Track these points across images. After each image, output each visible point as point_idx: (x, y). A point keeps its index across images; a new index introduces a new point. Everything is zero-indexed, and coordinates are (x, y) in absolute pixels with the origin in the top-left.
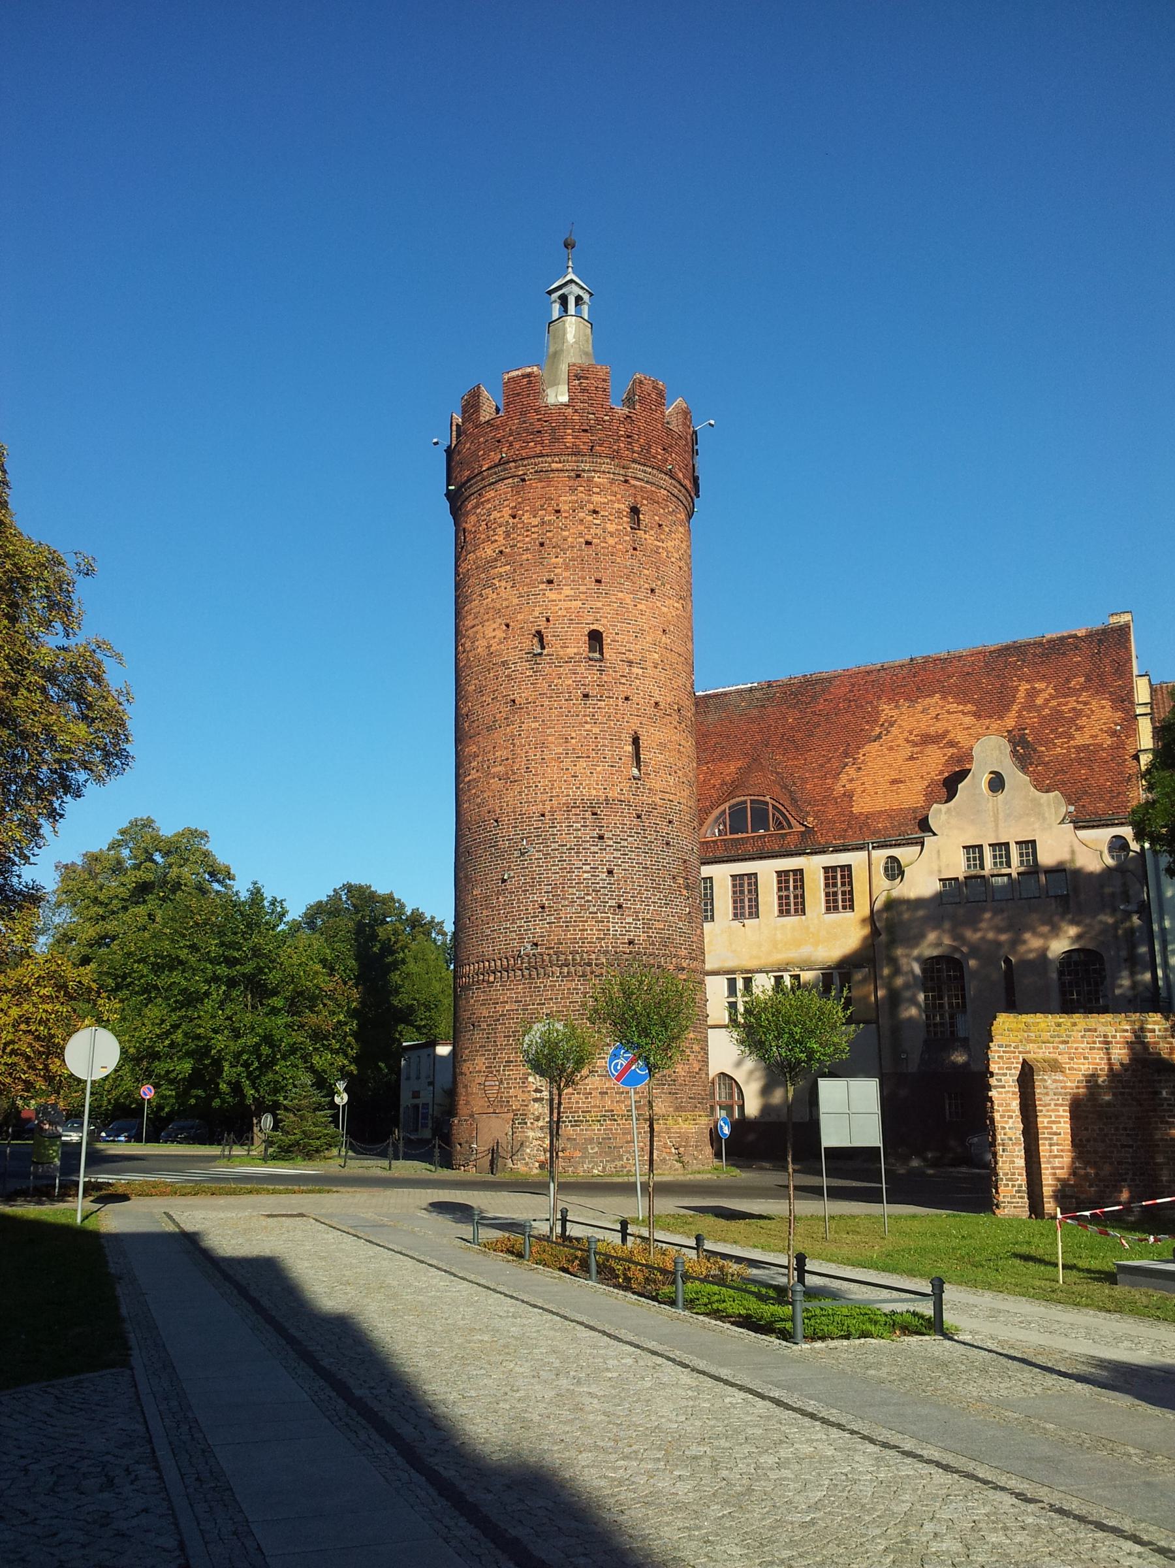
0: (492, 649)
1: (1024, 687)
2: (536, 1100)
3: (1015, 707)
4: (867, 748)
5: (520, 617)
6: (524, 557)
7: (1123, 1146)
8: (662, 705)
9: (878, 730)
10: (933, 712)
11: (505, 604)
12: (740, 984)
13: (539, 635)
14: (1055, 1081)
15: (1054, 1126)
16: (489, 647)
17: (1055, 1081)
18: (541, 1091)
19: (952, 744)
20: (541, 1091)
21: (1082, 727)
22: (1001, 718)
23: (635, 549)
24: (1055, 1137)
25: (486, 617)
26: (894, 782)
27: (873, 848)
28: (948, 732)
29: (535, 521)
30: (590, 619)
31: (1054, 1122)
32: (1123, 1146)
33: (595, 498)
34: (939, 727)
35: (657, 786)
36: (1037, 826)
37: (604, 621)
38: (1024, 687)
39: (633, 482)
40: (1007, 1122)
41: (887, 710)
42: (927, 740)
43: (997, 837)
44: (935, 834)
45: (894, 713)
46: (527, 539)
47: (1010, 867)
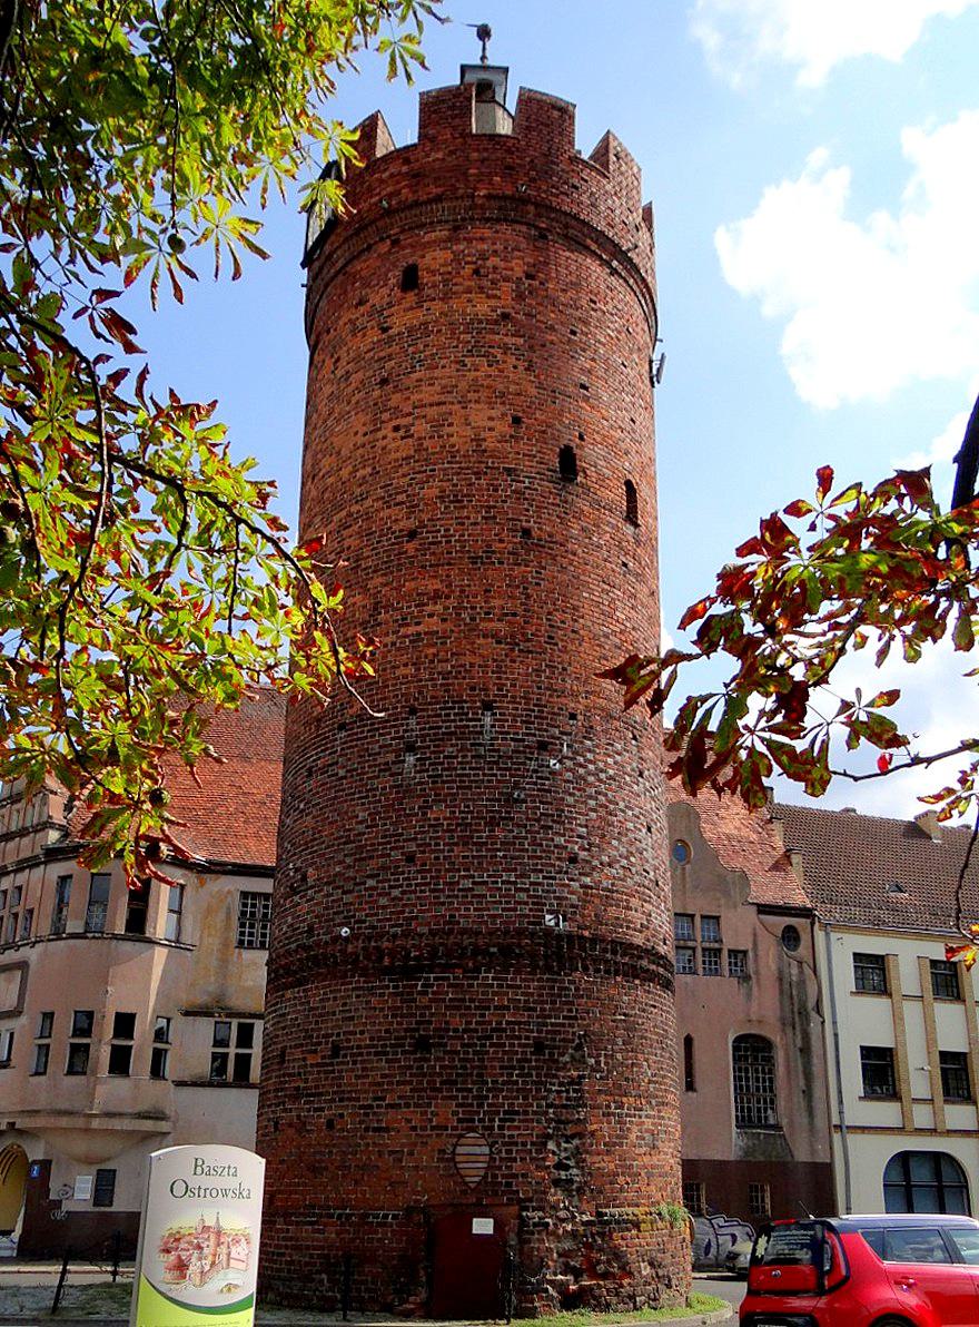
2: (557, 1183)
20: (567, 1168)
36: (723, 901)
43: (684, 908)
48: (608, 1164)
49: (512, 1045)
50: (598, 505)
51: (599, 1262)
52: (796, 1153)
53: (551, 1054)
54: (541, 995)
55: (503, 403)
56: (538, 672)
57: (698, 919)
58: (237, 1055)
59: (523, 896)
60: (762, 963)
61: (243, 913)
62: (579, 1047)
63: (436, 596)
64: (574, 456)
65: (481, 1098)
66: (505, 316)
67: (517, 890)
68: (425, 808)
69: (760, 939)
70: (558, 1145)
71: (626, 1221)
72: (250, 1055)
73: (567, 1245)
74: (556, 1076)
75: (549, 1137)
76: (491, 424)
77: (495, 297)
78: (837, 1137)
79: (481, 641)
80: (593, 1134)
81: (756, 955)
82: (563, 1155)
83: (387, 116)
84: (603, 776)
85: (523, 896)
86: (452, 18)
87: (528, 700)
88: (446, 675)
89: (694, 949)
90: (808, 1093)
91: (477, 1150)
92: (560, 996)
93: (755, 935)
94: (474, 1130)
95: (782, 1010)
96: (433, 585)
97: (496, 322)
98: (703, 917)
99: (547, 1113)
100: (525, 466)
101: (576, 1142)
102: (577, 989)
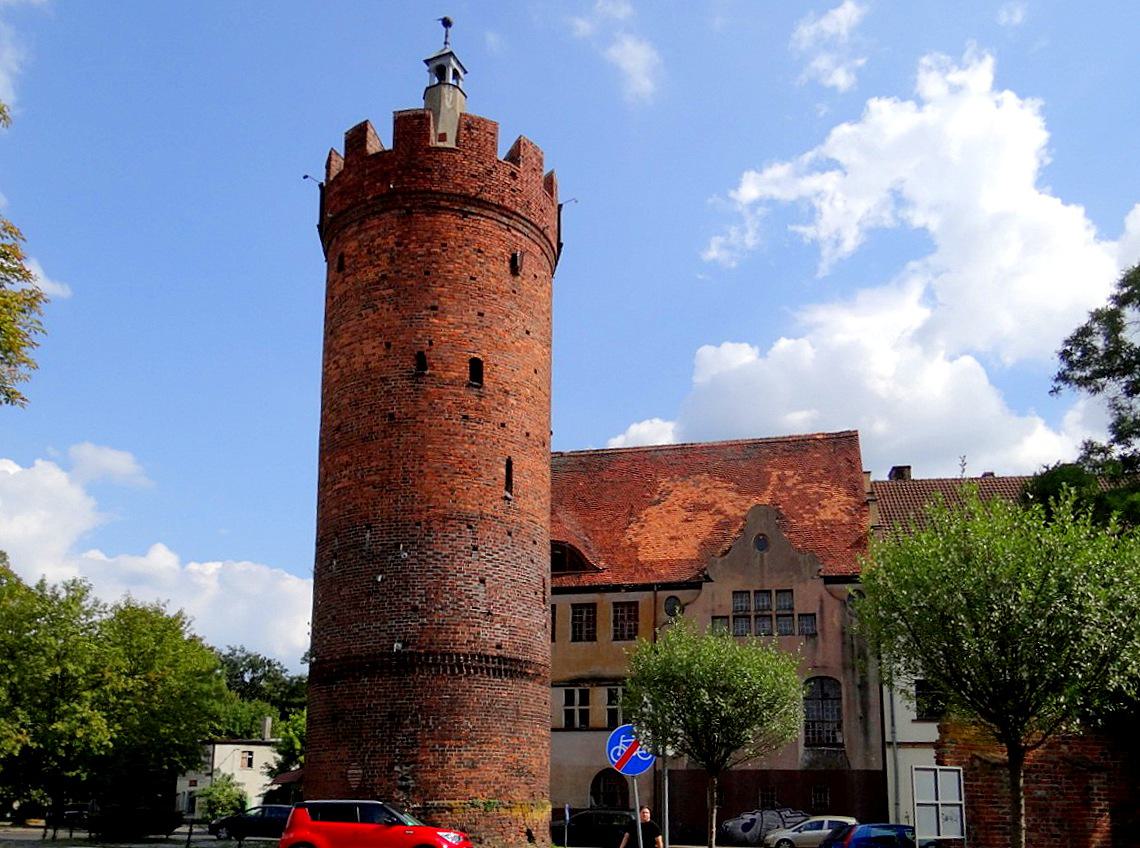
0: (372, 365)
1: (775, 473)
2: (401, 788)
4: (649, 510)
5: (402, 337)
6: (409, 283)
7: (1053, 836)
8: (532, 436)
9: (657, 497)
10: (703, 486)
16: (367, 363)
18: (408, 779)
19: (719, 512)
21: (824, 507)
22: (759, 495)
25: (365, 335)
27: (659, 589)
28: (716, 502)
32: (1053, 836)
34: (709, 499)
35: (526, 508)
36: (795, 577)
37: (485, 352)
38: (775, 473)
41: (664, 483)
42: (698, 507)
43: (763, 586)
44: (712, 581)
46: (412, 267)
47: (748, 592)
48: (432, 778)
49: (376, 716)
50: (443, 384)
52: (852, 764)
53: (399, 720)
54: (393, 688)
55: (380, 336)
56: (396, 502)
57: (752, 594)
58: (574, 710)
59: (384, 634)
60: (828, 621)
61: (616, 617)
62: (416, 715)
63: (348, 465)
64: (424, 357)
65: (360, 745)
66: (384, 277)
67: (381, 631)
68: (340, 589)
69: (825, 603)
70: (401, 768)
72: (588, 710)
75: (396, 764)
76: (374, 351)
77: (379, 265)
78: (889, 752)
79: (366, 489)
80: (423, 762)
81: (822, 618)
82: (405, 773)
83: (373, 122)
84: (439, 557)
85: (384, 634)
87: (389, 519)
88: (349, 511)
89: (771, 616)
90: (864, 719)
91: (356, 772)
92: (404, 687)
93: (822, 601)
94: (355, 761)
95: (843, 656)
96: (345, 458)
97: (378, 283)
98: (777, 592)
99: (394, 752)
100: (393, 374)
101: (412, 766)
102: (415, 683)
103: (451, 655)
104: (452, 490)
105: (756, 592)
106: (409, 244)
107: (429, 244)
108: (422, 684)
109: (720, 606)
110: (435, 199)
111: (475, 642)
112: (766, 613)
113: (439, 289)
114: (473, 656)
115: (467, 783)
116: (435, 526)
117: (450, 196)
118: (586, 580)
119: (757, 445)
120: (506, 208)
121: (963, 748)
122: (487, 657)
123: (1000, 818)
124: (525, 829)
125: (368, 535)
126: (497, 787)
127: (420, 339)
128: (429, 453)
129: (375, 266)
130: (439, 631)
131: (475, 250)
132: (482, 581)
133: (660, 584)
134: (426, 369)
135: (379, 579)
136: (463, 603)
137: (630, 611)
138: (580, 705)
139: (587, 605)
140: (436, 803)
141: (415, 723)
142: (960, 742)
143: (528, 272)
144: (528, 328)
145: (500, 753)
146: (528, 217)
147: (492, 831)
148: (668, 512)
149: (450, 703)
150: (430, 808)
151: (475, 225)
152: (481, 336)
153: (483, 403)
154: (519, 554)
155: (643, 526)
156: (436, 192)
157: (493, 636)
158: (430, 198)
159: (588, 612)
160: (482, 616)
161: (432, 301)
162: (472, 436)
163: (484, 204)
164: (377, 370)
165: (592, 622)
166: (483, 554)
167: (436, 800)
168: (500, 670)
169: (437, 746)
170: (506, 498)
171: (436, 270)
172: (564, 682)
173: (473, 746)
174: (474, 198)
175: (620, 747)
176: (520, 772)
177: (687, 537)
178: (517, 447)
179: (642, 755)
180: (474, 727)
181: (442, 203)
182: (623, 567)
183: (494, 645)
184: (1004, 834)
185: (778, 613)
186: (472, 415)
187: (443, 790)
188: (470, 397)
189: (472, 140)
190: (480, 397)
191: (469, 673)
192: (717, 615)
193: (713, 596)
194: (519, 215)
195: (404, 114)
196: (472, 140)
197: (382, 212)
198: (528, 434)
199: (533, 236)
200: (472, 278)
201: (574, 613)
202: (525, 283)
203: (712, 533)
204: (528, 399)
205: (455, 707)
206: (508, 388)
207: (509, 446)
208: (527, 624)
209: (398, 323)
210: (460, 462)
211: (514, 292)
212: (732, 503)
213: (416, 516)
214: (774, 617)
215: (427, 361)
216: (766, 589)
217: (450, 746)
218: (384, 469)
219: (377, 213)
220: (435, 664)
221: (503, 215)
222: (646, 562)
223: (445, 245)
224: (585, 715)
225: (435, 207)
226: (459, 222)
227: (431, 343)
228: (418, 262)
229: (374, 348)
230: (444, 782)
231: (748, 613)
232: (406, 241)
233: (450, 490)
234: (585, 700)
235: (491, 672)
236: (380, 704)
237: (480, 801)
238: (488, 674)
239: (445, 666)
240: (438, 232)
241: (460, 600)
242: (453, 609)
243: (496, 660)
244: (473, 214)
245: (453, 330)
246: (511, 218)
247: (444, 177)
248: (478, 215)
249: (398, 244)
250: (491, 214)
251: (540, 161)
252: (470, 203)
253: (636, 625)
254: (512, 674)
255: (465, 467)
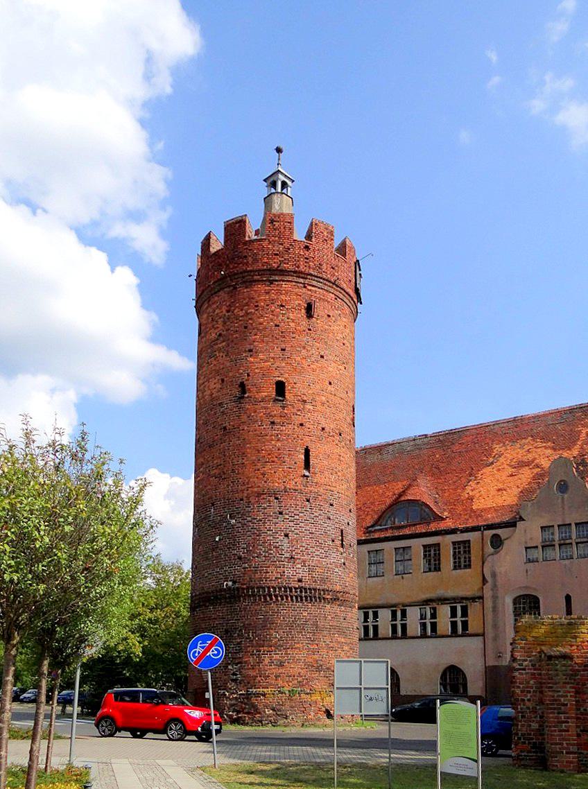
3: (579, 443)
4: (484, 470)
5: (231, 374)
8: (327, 429)
9: (491, 460)
10: (526, 448)
11: (222, 367)
12: (399, 614)
13: (242, 385)
14: (564, 665)
15: (562, 699)
17: (564, 665)
18: (236, 675)
19: (537, 466)
20: (236, 675)
22: (570, 449)
23: (310, 330)
24: (563, 708)
25: (210, 376)
26: (499, 490)
27: (484, 529)
28: (535, 459)
29: (241, 313)
30: (277, 373)
31: (562, 696)
33: (283, 297)
34: (530, 457)
35: (322, 481)
39: (309, 288)
40: (526, 696)
41: (497, 448)
42: (522, 464)
45: (502, 449)
47: (553, 526)
48: (251, 673)
50: (257, 402)
51: (245, 708)
53: (231, 634)
56: (228, 486)
59: (221, 576)
61: (455, 553)
62: (241, 630)
71: (258, 694)
73: (233, 702)
74: (232, 642)
75: (229, 664)
80: (246, 662)
84: (255, 521)
85: (221, 576)
86: (114, 274)
87: (224, 498)
89: (571, 544)
97: (217, 339)
98: (577, 524)
103: (264, 588)
104: (264, 474)
105: (559, 526)
106: (234, 310)
107: (246, 307)
108: (245, 609)
109: (531, 539)
110: (250, 275)
111: (280, 578)
112: (568, 541)
113: (253, 337)
114: (280, 588)
115: (276, 677)
116: (252, 500)
117: (261, 272)
118: (433, 527)
119: (571, 410)
120: (302, 273)
121: (534, 644)
122: (291, 589)
123: (556, 700)
124: (324, 709)
125: (212, 510)
126: (300, 679)
127: (242, 374)
128: (248, 450)
129: (215, 329)
130: (256, 572)
131: (278, 305)
132: (286, 535)
133: (485, 526)
134: (245, 393)
135: (217, 539)
136: (272, 552)
137: (465, 547)
138: (462, 617)
139: (464, 542)
140: (255, 690)
141: (240, 636)
142: (530, 639)
143: (321, 313)
144: (322, 353)
145: (302, 655)
146: (320, 275)
147: (295, 711)
148: (499, 470)
149: (263, 621)
150: (250, 694)
151: (279, 288)
152: (284, 364)
153: (286, 411)
154: (316, 514)
155: (479, 483)
156: (251, 271)
157: (294, 573)
158: (247, 276)
159: (435, 550)
160: (286, 560)
161: (248, 346)
162: (277, 435)
163: (283, 272)
164: (218, 398)
165: (438, 557)
166: (287, 517)
167: (255, 688)
168: (301, 597)
169: (255, 651)
170: (304, 476)
171: (252, 324)
172: (418, 602)
173: (280, 651)
174: (277, 270)
175: (198, 650)
176: (319, 669)
177: (510, 488)
178: (313, 438)
179: (214, 655)
180: (281, 637)
181: (255, 277)
182: (461, 515)
183: (296, 579)
184: (559, 713)
185: (577, 541)
186: (277, 420)
187: (259, 682)
188: (276, 409)
189: (275, 229)
190: (283, 408)
191: (277, 600)
192: (529, 545)
193: (525, 531)
194: (311, 275)
195: (230, 222)
196: (275, 229)
197: (219, 291)
198: (323, 429)
199: (326, 288)
200: (276, 326)
201: (425, 551)
202: (319, 322)
203: (530, 483)
204: (323, 404)
205: (267, 624)
206: (305, 398)
207: (307, 439)
208: (325, 563)
209: (228, 364)
210: (269, 454)
211: (310, 330)
212: (545, 457)
213: (240, 495)
214: (574, 544)
215: (247, 387)
216: (567, 523)
217: (264, 652)
218: (221, 465)
219: (215, 293)
220: (254, 595)
221: (299, 277)
222: (478, 509)
223: (257, 306)
224: (434, 626)
225: (250, 282)
226: (267, 288)
227: (248, 375)
228: (240, 320)
229: (215, 384)
230: (260, 676)
231: (554, 543)
232: (233, 308)
233: (262, 474)
234: (465, 613)
235: (294, 598)
236: (220, 624)
237: (286, 689)
238: (292, 600)
239: (260, 596)
240: (253, 298)
241: (271, 550)
242: (265, 556)
243: (298, 590)
244: (276, 281)
245: (263, 365)
246: (306, 278)
247: (256, 261)
248: (280, 281)
249: (228, 311)
250: (290, 278)
251: (332, 233)
252: (274, 274)
253: (470, 558)
254: (310, 599)
255: (273, 457)
